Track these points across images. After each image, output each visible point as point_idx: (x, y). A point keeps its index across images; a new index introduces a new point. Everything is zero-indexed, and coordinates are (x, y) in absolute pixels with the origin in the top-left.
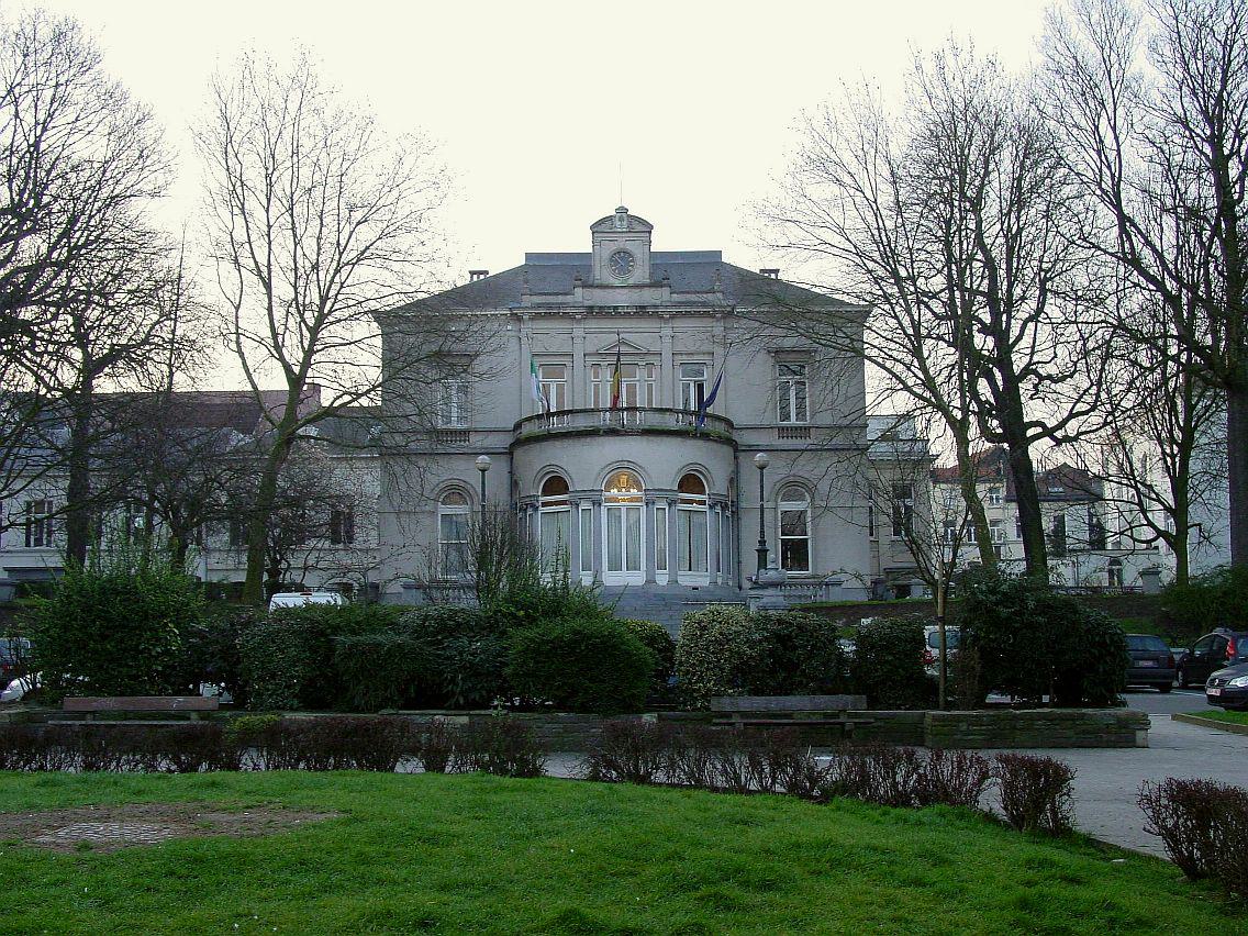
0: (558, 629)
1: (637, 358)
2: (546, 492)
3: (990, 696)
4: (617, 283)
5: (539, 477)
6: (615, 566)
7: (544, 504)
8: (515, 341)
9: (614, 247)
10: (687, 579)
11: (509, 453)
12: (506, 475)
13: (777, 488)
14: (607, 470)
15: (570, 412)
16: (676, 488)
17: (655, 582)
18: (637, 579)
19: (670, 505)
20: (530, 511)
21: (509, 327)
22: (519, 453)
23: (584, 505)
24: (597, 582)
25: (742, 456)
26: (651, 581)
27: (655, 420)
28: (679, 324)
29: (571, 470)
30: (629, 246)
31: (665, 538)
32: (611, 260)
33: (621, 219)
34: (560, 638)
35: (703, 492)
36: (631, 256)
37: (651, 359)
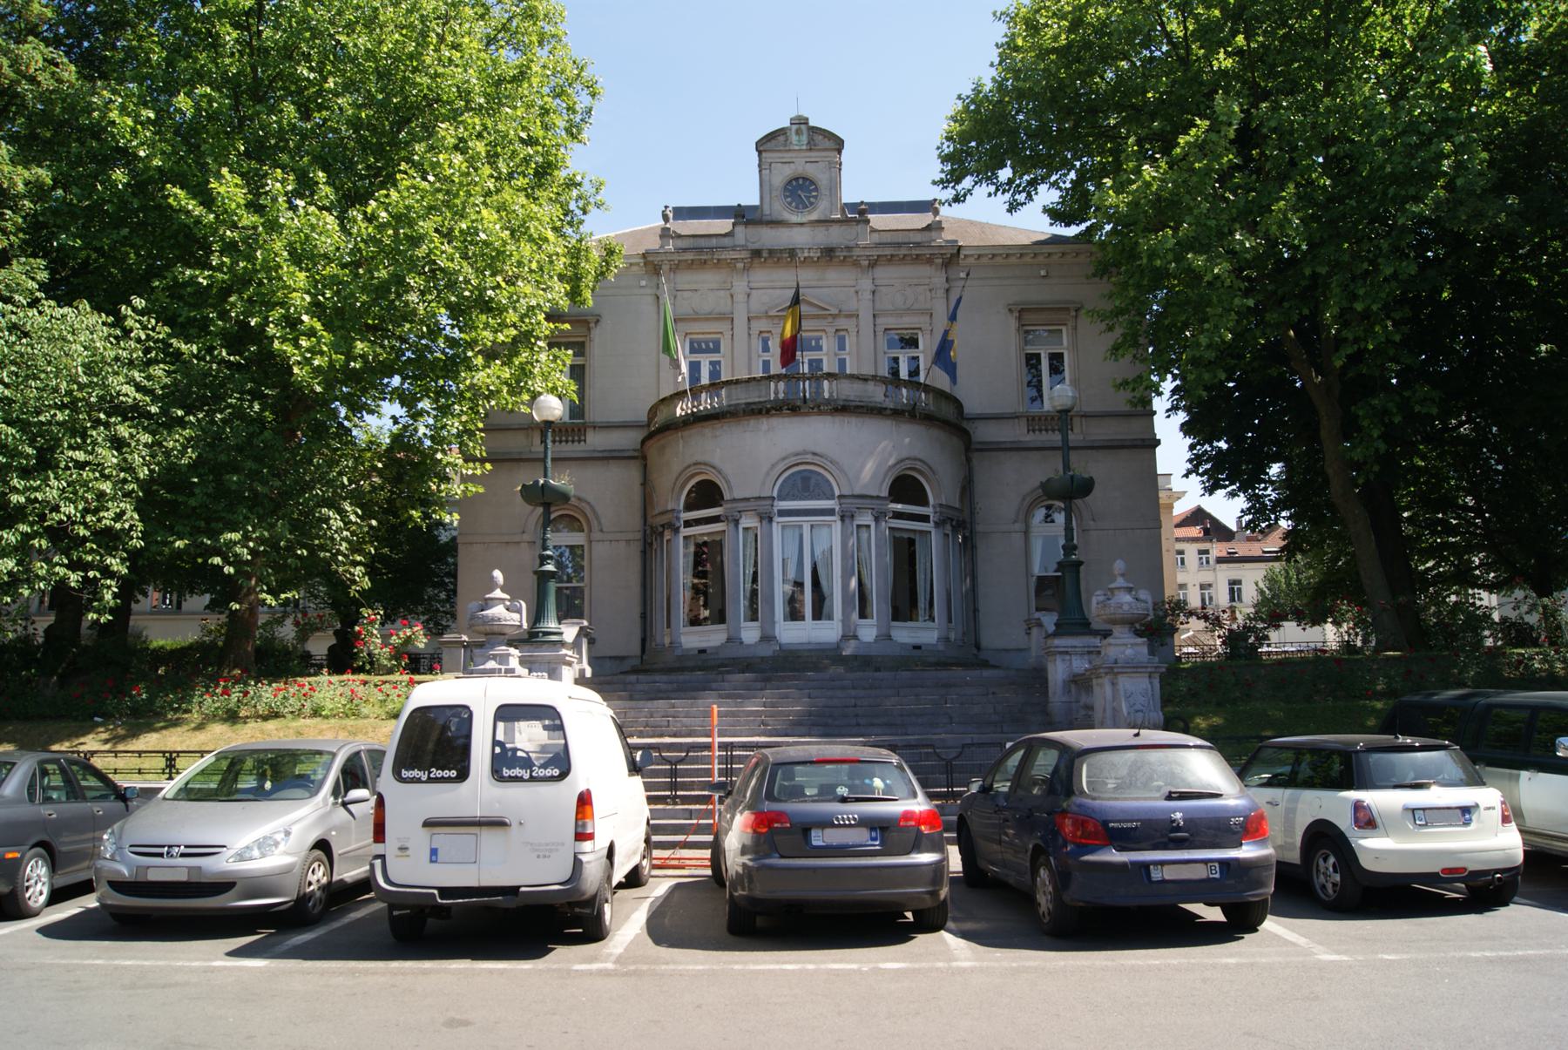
0: (968, 926)
1: (824, 322)
2: (689, 507)
3: (1006, 789)
4: (795, 219)
5: (681, 480)
6: (794, 614)
7: (688, 524)
8: (651, 299)
9: (787, 172)
10: (906, 634)
11: (641, 457)
12: (637, 489)
13: (1026, 503)
14: (781, 467)
15: (728, 383)
16: (885, 493)
17: (855, 637)
18: (826, 632)
19: (877, 519)
20: (667, 535)
21: (643, 283)
22: (652, 449)
23: (748, 521)
24: (767, 638)
25: (976, 457)
26: (849, 635)
27: (849, 391)
28: (884, 273)
29: (727, 469)
30: (811, 171)
31: (788, 744)
32: (785, 189)
33: (798, 132)
34: (97, 308)
35: (924, 502)
36: (812, 183)
37: (842, 323)
